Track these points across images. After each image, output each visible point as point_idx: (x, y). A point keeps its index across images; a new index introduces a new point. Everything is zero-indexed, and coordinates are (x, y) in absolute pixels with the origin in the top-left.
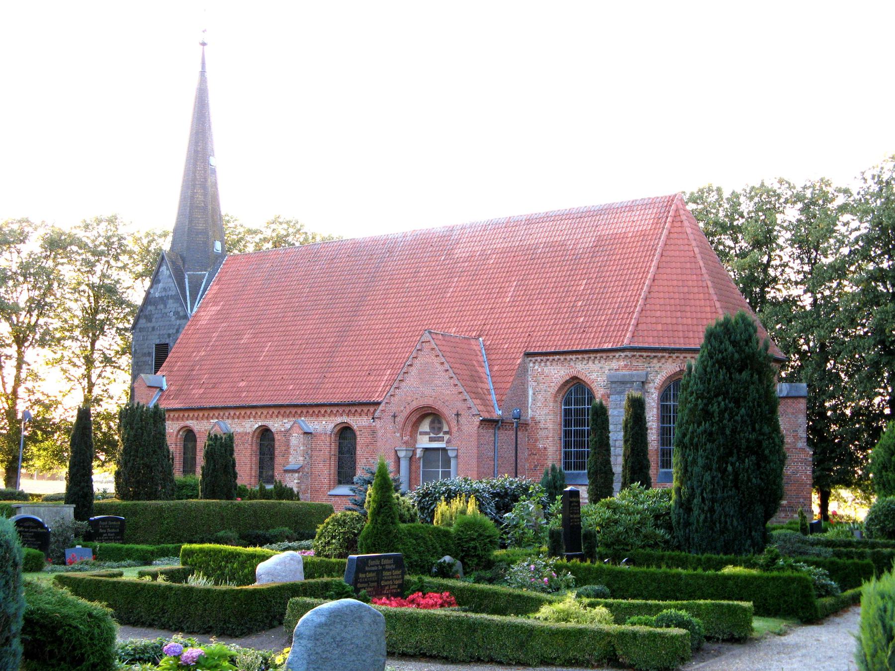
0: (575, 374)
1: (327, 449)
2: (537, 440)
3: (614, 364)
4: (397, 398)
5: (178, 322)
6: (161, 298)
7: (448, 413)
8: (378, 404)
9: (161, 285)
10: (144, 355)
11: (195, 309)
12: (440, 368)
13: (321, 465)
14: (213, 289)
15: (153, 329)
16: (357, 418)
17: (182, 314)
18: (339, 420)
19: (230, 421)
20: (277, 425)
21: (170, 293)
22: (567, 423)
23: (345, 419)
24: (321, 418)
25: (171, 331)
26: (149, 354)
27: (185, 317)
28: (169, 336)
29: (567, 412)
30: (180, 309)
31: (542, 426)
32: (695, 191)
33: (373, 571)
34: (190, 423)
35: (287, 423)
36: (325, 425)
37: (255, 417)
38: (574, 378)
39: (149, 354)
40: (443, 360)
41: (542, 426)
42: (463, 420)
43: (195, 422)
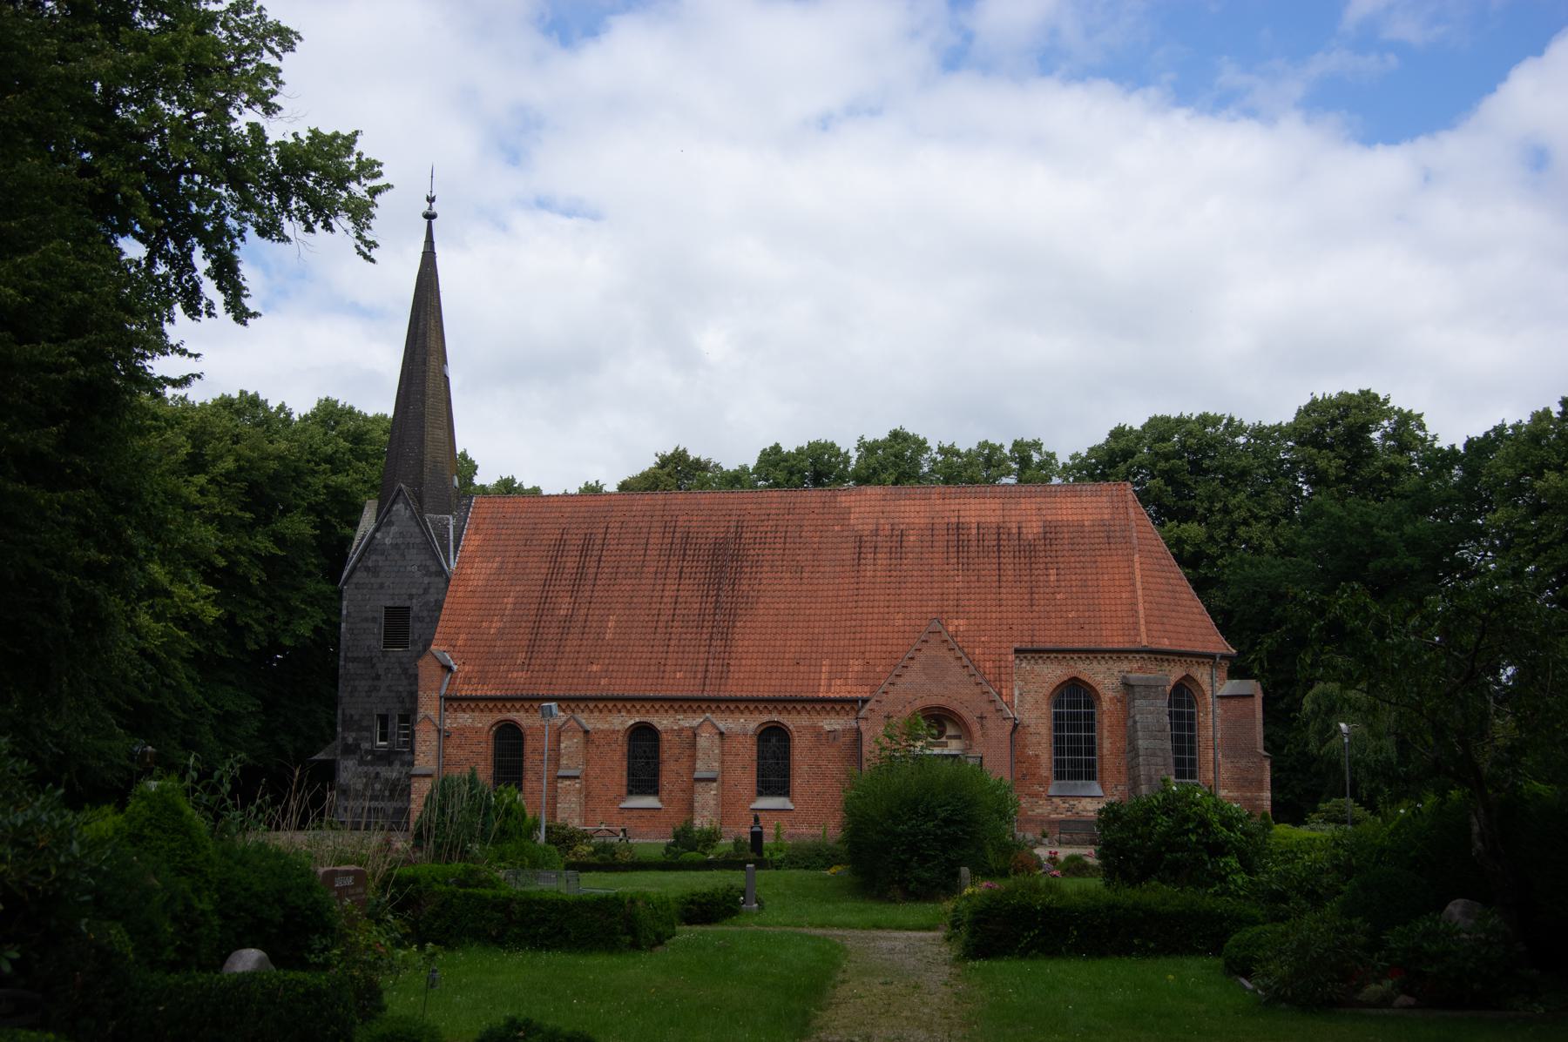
0: (1075, 674)
1: (747, 752)
2: (1025, 746)
3: (1125, 666)
4: (891, 695)
5: (426, 580)
6: (396, 546)
7: (969, 716)
8: (865, 701)
9: (394, 529)
10: (366, 620)
11: (453, 565)
12: (955, 663)
13: (739, 772)
14: (471, 541)
15: (382, 586)
16: (794, 716)
17: (433, 569)
18: (766, 718)
19: (586, 715)
20: (663, 722)
21: (412, 540)
22: (1058, 727)
23: (775, 717)
24: (737, 715)
25: (414, 591)
26: (374, 620)
27: (441, 572)
28: (411, 597)
29: (1057, 716)
30: (429, 563)
31: (1032, 730)
32: (974, 447)
33: (347, 873)
34: (513, 716)
35: (689, 721)
36: (747, 724)
37: (629, 711)
38: (1075, 678)
39: (374, 620)
40: (960, 654)
41: (1032, 730)
42: (989, 723)
43: (522, 714)
